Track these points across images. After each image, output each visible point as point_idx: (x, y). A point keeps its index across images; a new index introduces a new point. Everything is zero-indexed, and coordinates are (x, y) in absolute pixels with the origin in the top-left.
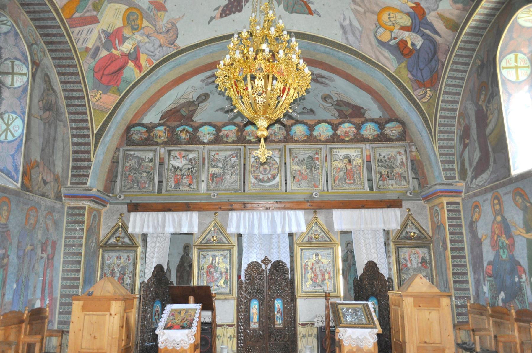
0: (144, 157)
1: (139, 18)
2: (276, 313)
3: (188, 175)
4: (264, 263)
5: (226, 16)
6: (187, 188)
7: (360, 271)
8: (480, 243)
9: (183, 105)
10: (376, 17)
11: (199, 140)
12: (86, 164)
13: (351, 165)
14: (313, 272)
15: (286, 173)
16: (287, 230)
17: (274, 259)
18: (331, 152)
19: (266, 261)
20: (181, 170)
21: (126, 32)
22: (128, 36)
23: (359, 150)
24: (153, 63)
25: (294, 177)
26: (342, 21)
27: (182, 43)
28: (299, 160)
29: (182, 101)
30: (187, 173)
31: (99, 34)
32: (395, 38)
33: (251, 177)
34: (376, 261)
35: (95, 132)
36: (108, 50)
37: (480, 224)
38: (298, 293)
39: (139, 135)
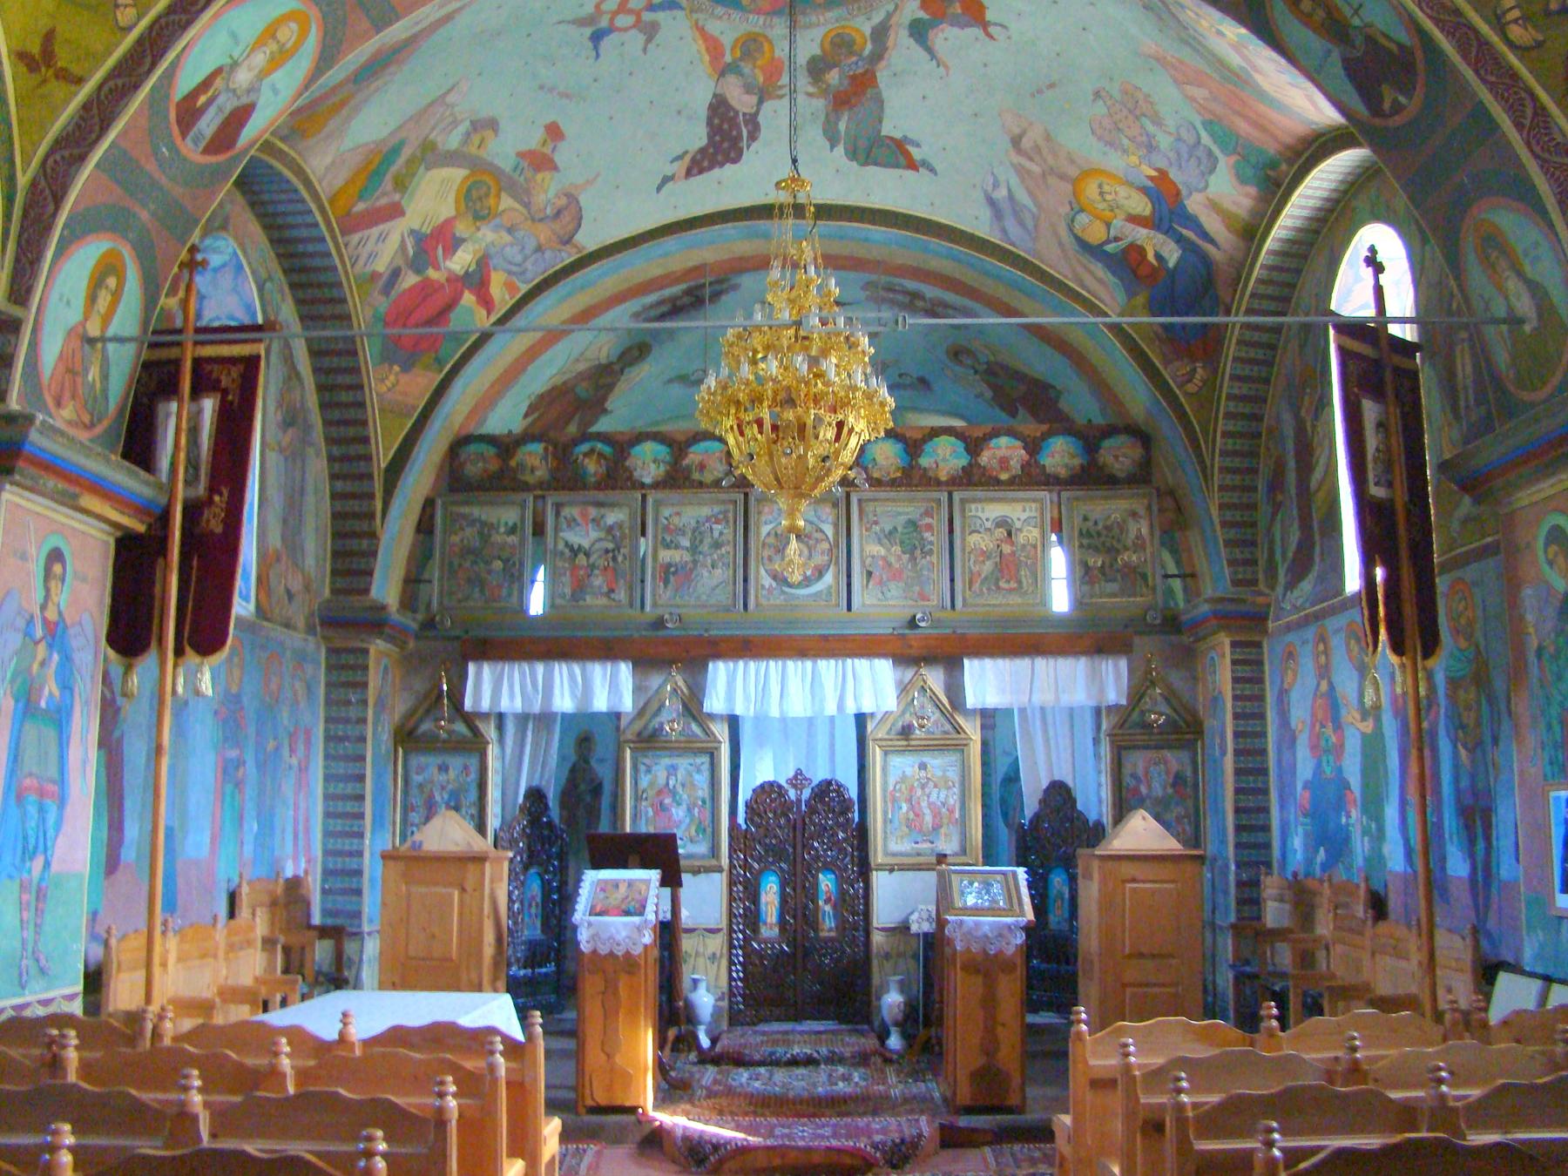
0: (495, 521)
1: (493, 191)
2: (821, 903)
3: (605, 569)
4: (795, 786)
5: (701, 172)
6: (603, 601)
7: (1031, 806)
8: (1293, 740)
9: (581, 376)
10: (1070, 187)
11: (630, 478)
12: (365, 544)
13: (1012, 544)
14: (912, 808)
15: (849, 576)
16: (851, 709)
17: (819, 774)
18: (963, 510)
19: (798, 779)
20: (587, 555)
21: (461, 229)
22: (465, 236)
23: (1034, 505)
24: (518, 289)
25: (870, 574)
26: (990, 188)
27: (589, 239)
28: (883, 530)
29: (581, 367)
30: (602, 562)
31: (403, 241)
32: (1117, 239)
33: (763, 572)
34: (1070, 782)
35: (383, 465)
36: (418, 271)
37: (1294, 696)
38: (878, 856)
39: (480, 464)
